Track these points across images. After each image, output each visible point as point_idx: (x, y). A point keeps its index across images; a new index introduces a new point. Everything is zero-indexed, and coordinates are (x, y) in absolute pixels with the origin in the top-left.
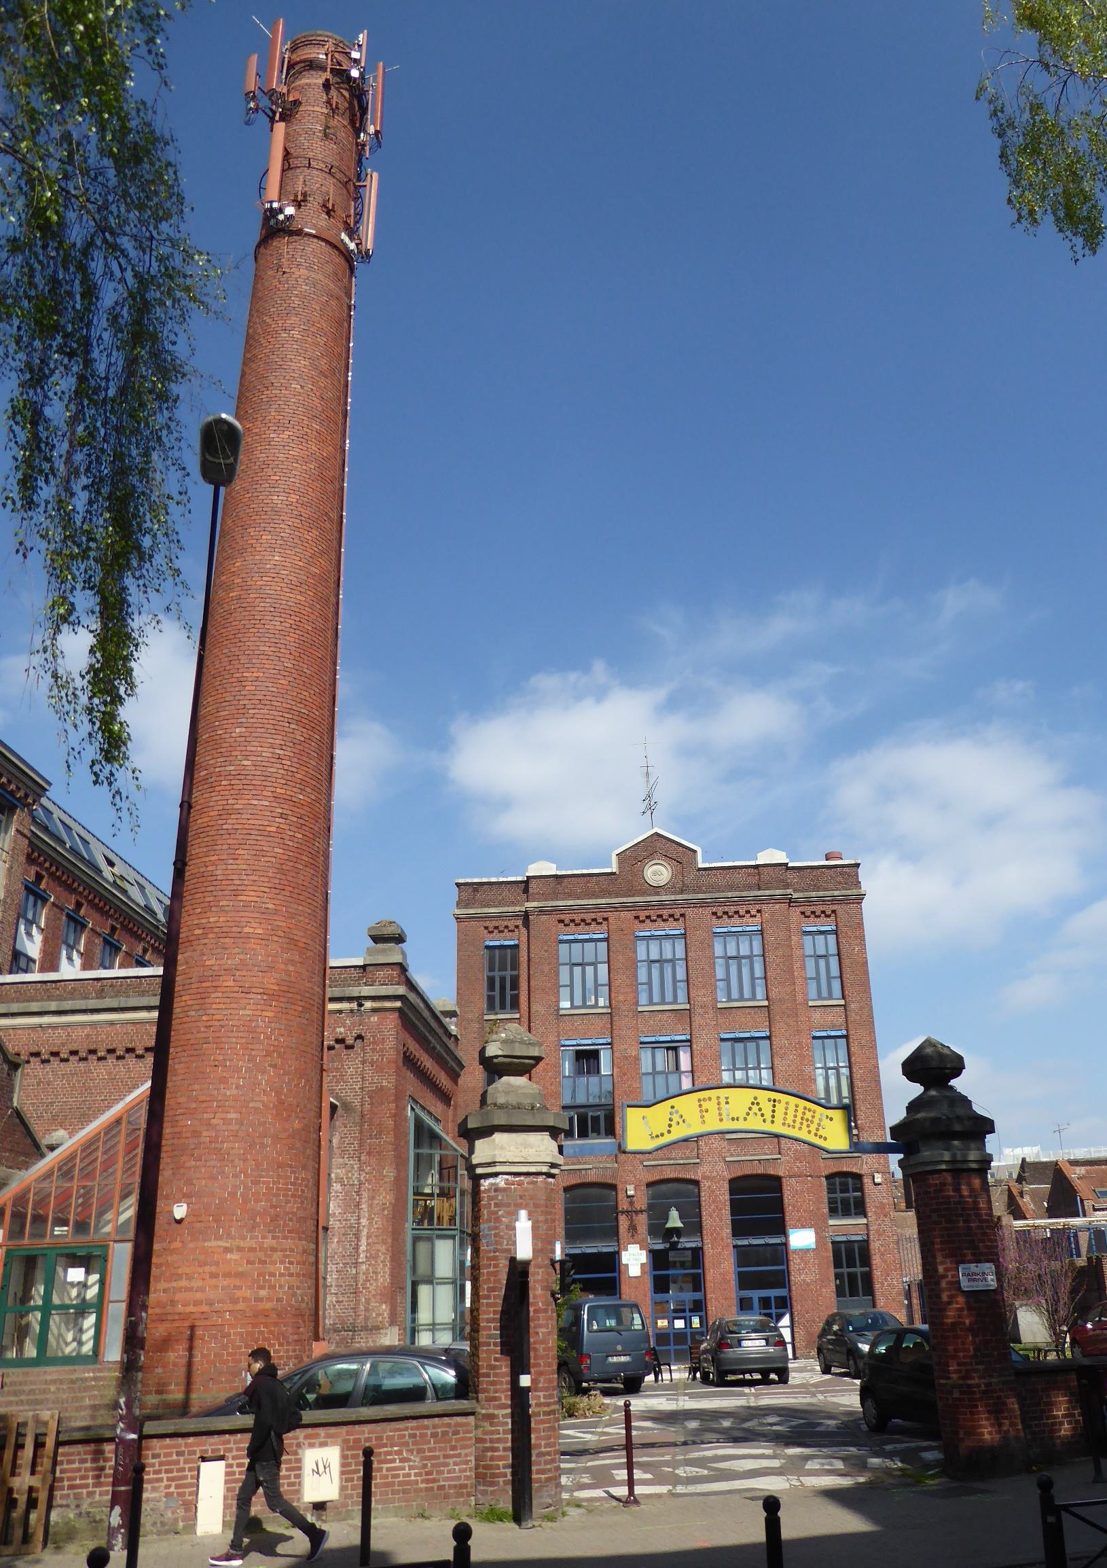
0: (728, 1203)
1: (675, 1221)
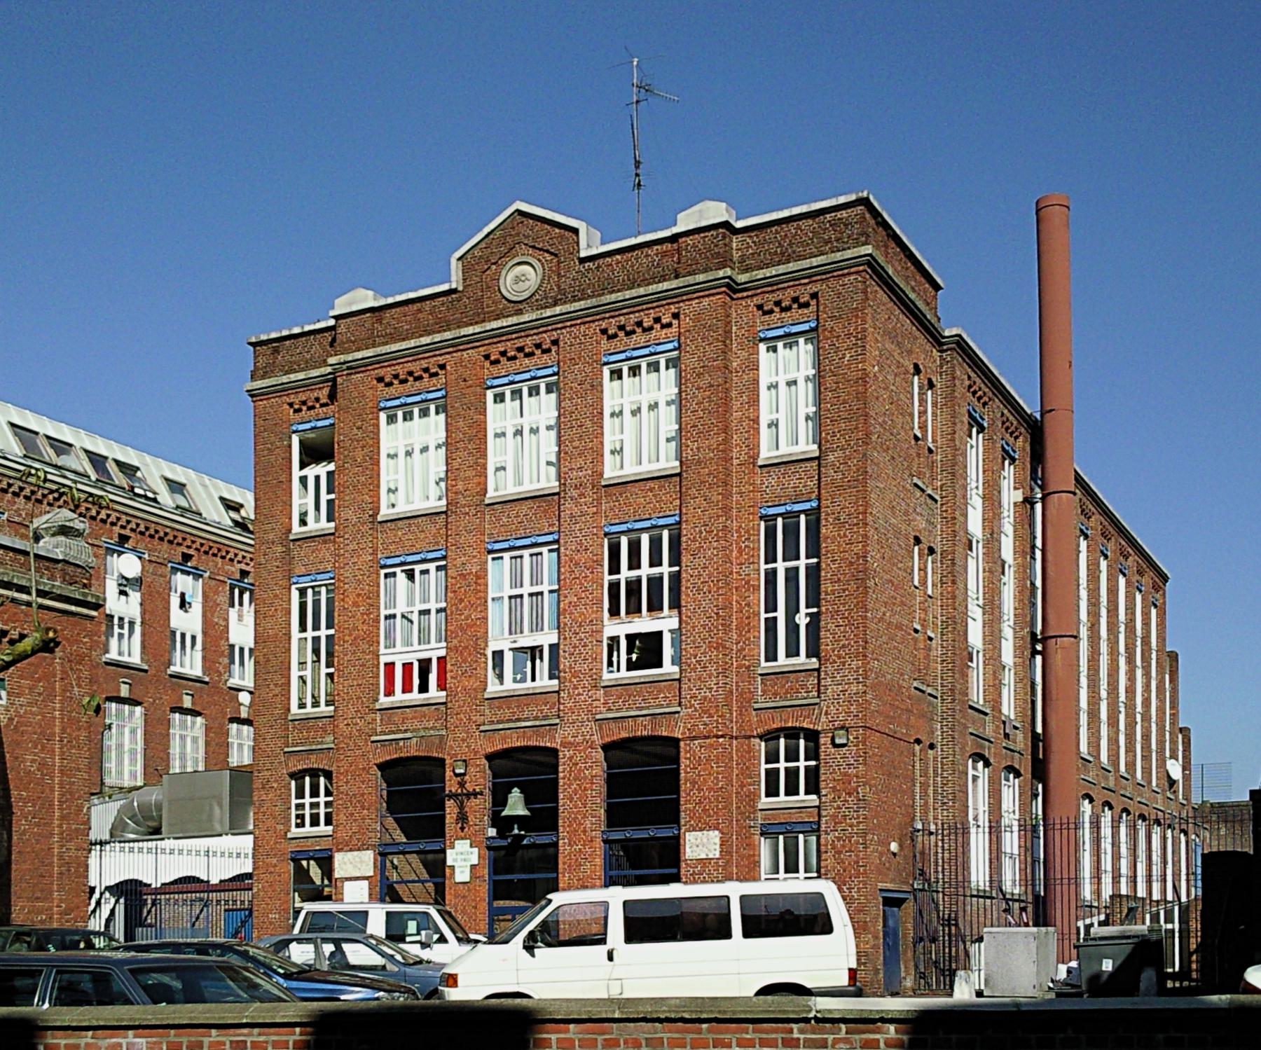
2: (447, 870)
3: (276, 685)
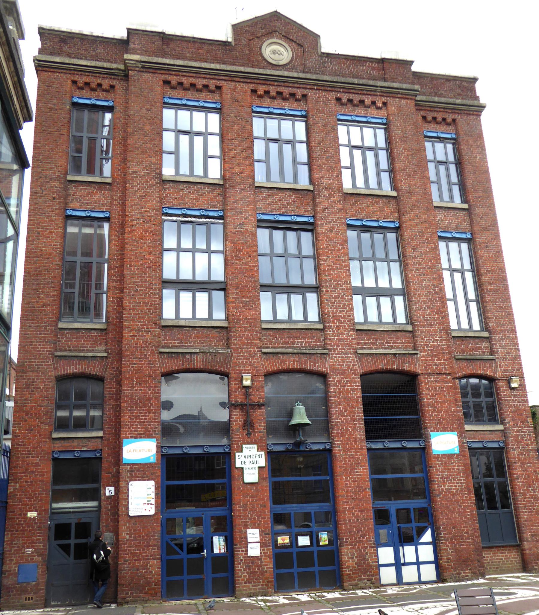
0: (360, 400)
1: (301, 417)
2: (236, 472)
3: (47, 296)
